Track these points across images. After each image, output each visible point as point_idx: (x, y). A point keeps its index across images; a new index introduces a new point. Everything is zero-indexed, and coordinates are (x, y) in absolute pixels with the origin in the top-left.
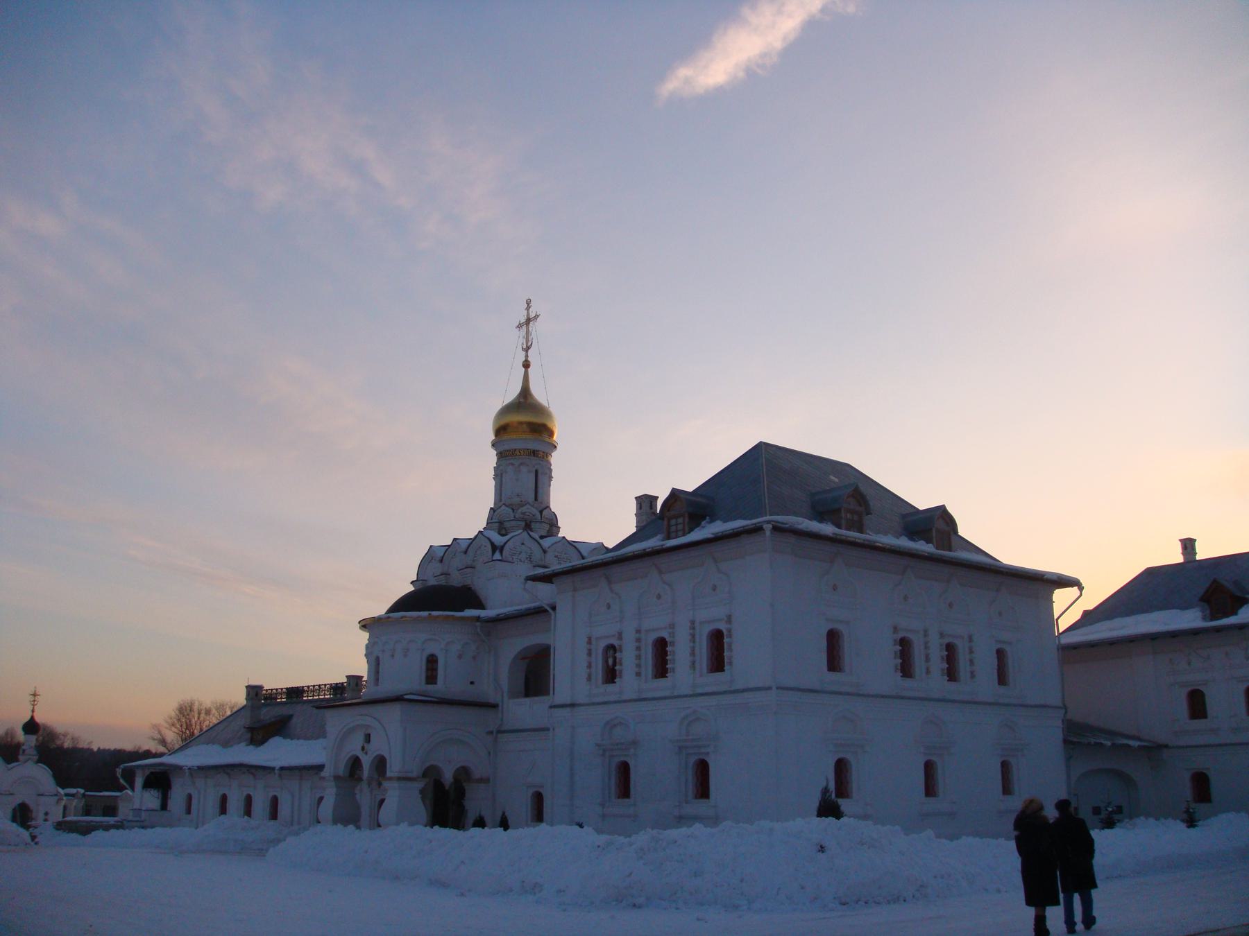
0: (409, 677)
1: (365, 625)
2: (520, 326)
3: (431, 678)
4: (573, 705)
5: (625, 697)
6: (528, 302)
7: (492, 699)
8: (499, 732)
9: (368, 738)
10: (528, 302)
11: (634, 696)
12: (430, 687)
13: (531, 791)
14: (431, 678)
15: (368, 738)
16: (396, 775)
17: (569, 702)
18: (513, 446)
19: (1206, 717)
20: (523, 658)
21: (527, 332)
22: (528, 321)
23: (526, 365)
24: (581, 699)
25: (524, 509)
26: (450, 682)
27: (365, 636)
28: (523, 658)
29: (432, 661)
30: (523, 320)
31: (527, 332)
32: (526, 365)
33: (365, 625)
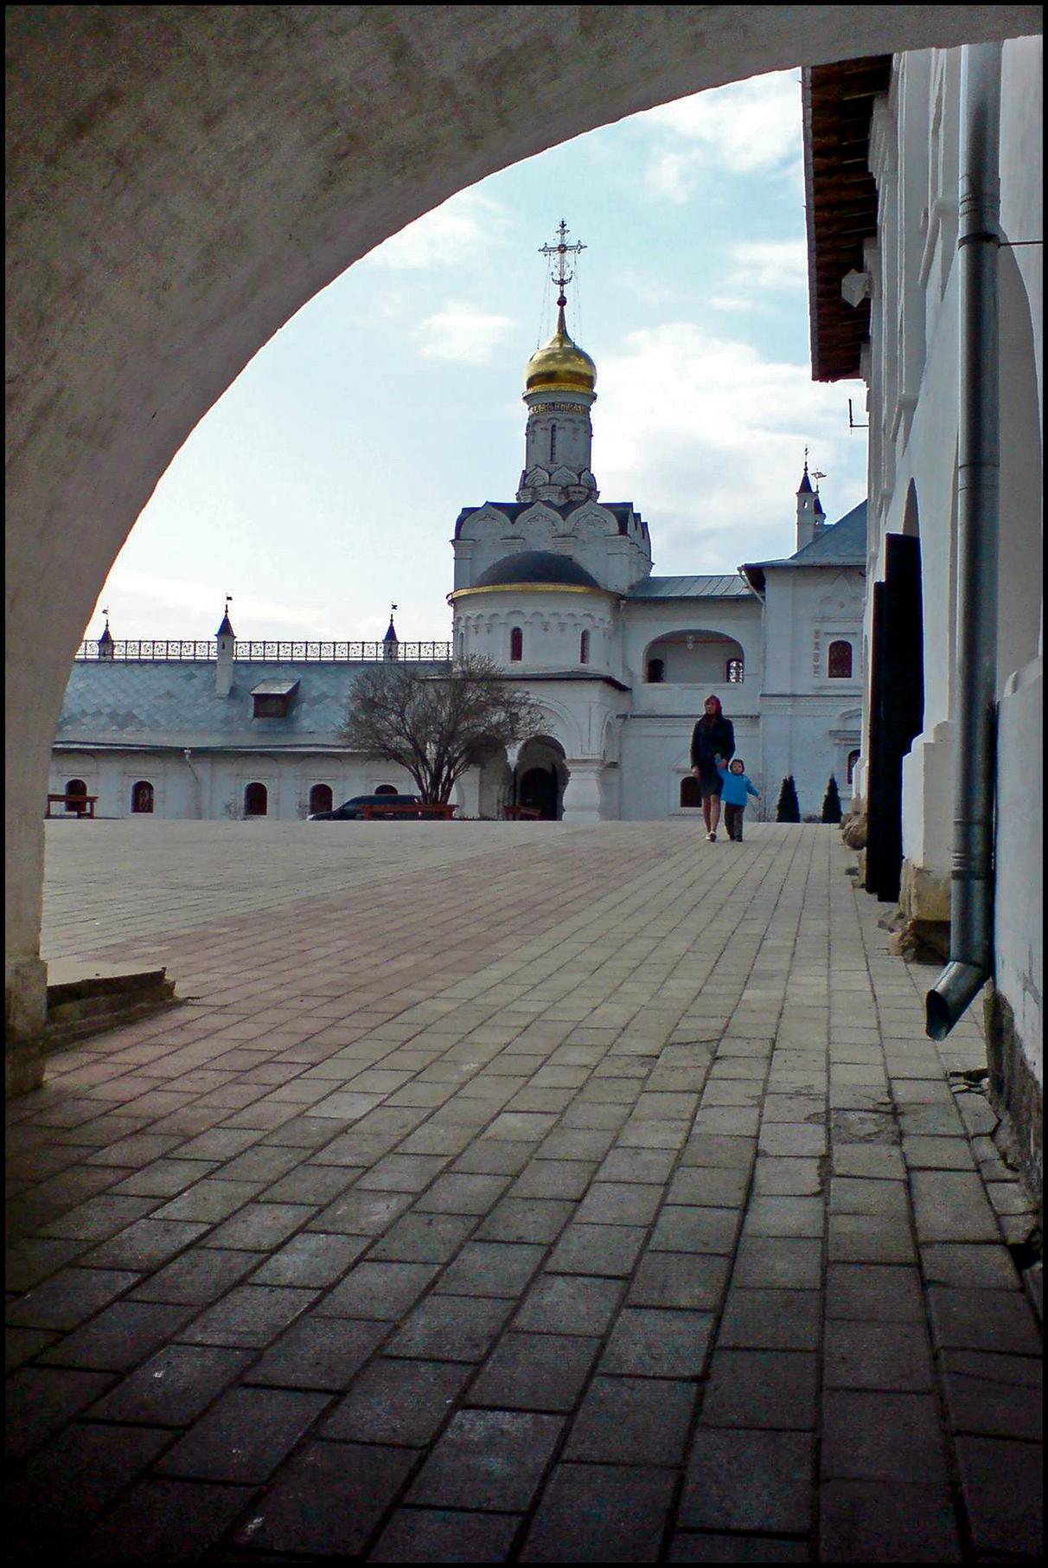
3: (517, 654)
14: (517, 654)
21: (562, 262)
31: (562, 262)
32: (562, 302)
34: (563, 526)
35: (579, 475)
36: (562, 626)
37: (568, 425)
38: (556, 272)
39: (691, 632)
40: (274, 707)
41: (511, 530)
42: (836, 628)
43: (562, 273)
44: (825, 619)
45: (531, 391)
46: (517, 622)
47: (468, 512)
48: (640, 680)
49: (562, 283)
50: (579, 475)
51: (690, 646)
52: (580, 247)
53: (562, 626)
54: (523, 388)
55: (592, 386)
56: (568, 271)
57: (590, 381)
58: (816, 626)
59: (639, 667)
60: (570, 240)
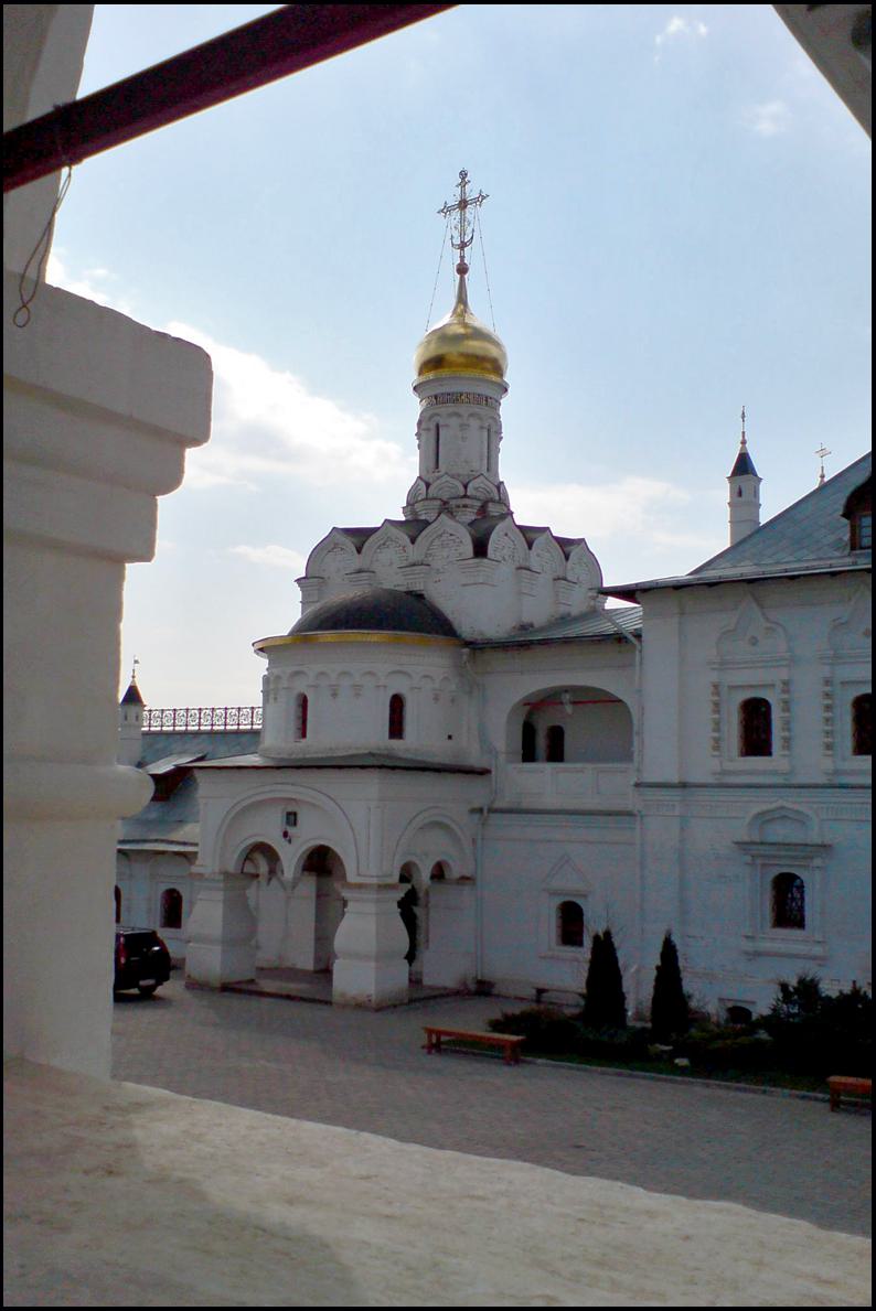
0: (352, 723)
1: (265, 648)
2: (446, 210)
3: (396, 729)
4: (684, 785)
5: (795, 781)
6: (463, 175)
7: (475, 759)
8: (491, 811)
9: (292, 818)
10: (463, 175)
11: (822, 780)
12: (395, 743)
13: (558, 901)
14: (396, 729)
15: (292, 818)
16: (375, 881)
17: (675, 780)
18: (455, 388)
19: (769, 753)
20: (525, 704)
21: (463, 220)
22: (463, 204)
23: (462, 270)
24: (696, 777)
25: (478, 480)
26: (421, 738)
27: (263, 663)
28: (525, 704)
29: (397, 704)
30: (453, 201)
31: (463, 220)
32: (462, 270)
33: (265, 648)
34: (415, 553)
35: (466, 487)
36: (357, 690)
37: (454, 421)
38: (456, 234)
39: (566, 690)
40: (292, 817)
41: (357, 562)
42: (740, 677)
43: (462, 234)
44: (723, 665)
45: (423, 379)
46: (301, 686)
47: (149, 560)
48: (502, 757)
49: (463, 246)
50: (466, 487)
51: (569, 709)
52: (482, 197)
53: (357, 690)
54: (413, 377)
55: (501, 375)
56: (469, 231)
57: (497, 367)
58: (714, 677)
59: (502, 734)
60: (472, 192)
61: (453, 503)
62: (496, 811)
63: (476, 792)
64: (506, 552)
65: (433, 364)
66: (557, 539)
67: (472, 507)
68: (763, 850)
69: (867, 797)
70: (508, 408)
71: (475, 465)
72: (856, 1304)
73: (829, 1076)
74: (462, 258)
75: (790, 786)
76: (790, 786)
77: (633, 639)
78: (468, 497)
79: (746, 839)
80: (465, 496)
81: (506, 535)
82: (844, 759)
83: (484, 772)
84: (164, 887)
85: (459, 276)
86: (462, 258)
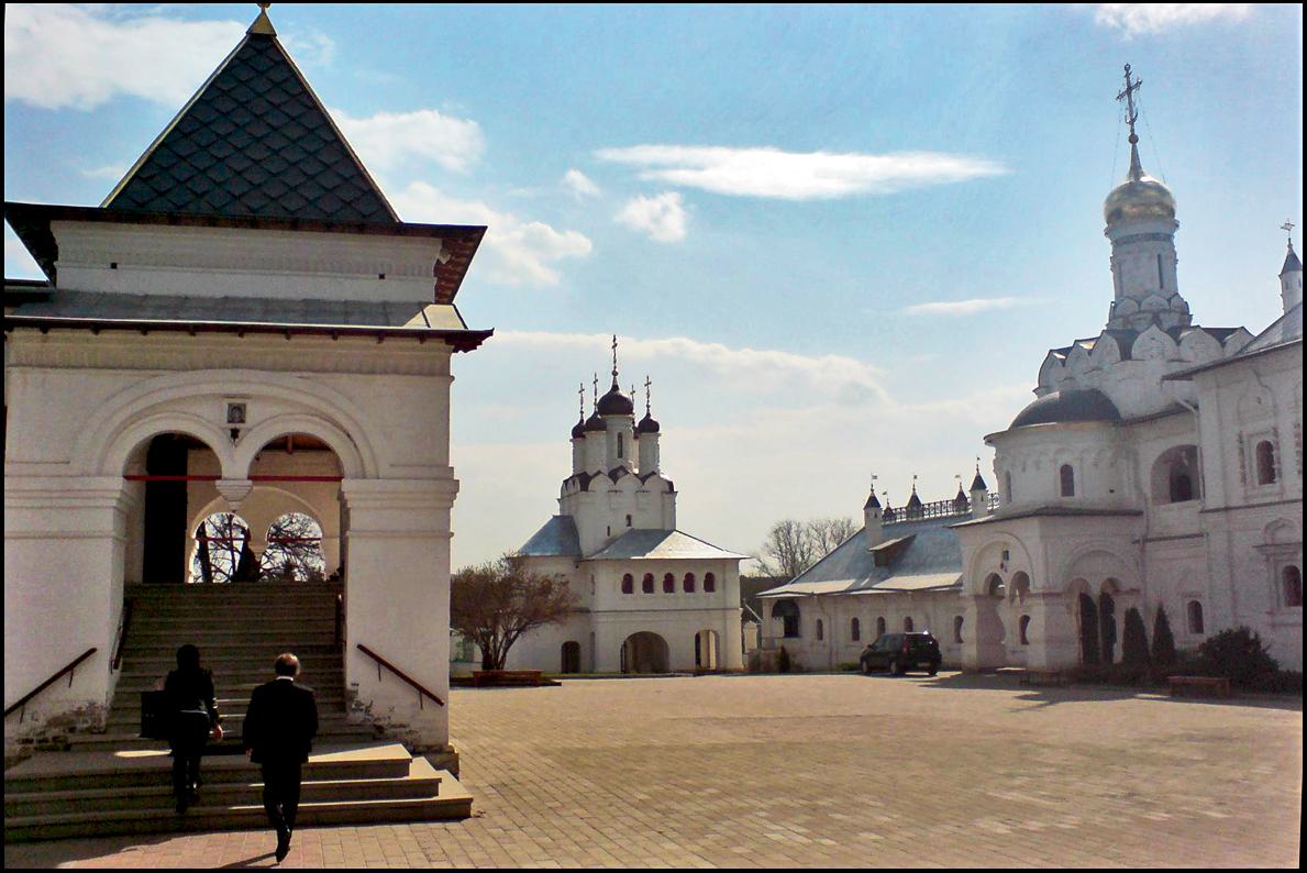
0: (1040, 486)
2: (1120, 97)
4: (1227, 509)
5: (1285, 498)
6: (1127, 68)
9: (1006, 555)
10: (1127, 68)
12: (1067, 499)
16: (1041, 591)
23: (1133, 139)
24: (1235, 502)
26: (1089, 491)
27: (992, 450)
31: (1130, 102)
35: (1140, 305)
49: (1132, 122)
50: (1140, 305)
61: (1131, 318)
62: (1151, 540)
63: (1137, 528)
64: (1154, 351)
65: (1114, 216)
66: (1208, 330)
67: (1145, 319)
68: (1272, 550)
69: (1300, 505)
70: (1179, 239)
71: (1149, 286)
72: (6, 860)
73: (309, 750)
74: (1132, 130)
75: (1284, 502)
76: (1284, 502)
77: (1193, 410)
78: (1144, 312)
79: (1262, 542)
80: (1140, 312)
81: (1153, 339)
82: (1254, 488)
83: (1139, 514)
84: (852, 617)
85: (1131, 145)
86: (1132, 130)
